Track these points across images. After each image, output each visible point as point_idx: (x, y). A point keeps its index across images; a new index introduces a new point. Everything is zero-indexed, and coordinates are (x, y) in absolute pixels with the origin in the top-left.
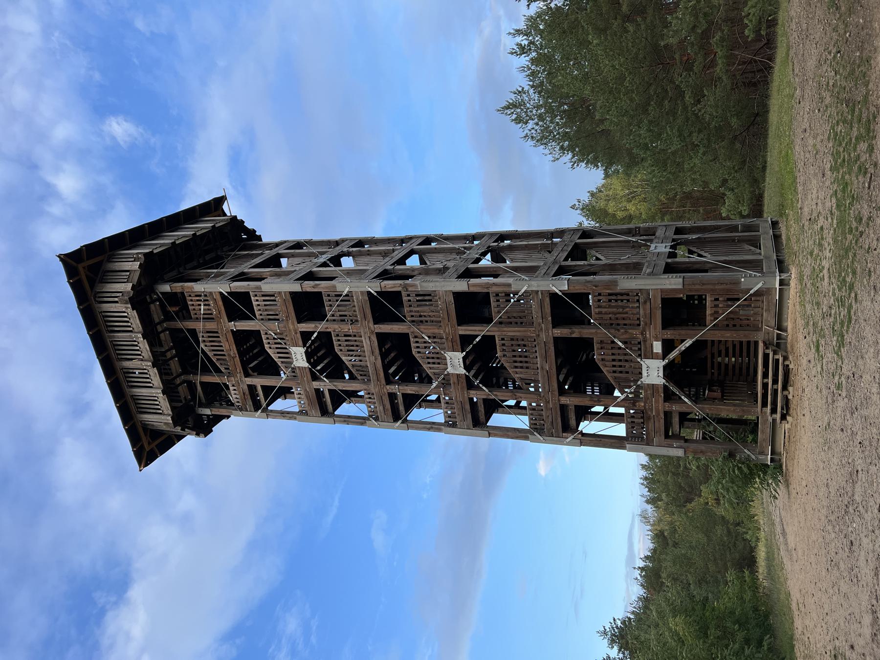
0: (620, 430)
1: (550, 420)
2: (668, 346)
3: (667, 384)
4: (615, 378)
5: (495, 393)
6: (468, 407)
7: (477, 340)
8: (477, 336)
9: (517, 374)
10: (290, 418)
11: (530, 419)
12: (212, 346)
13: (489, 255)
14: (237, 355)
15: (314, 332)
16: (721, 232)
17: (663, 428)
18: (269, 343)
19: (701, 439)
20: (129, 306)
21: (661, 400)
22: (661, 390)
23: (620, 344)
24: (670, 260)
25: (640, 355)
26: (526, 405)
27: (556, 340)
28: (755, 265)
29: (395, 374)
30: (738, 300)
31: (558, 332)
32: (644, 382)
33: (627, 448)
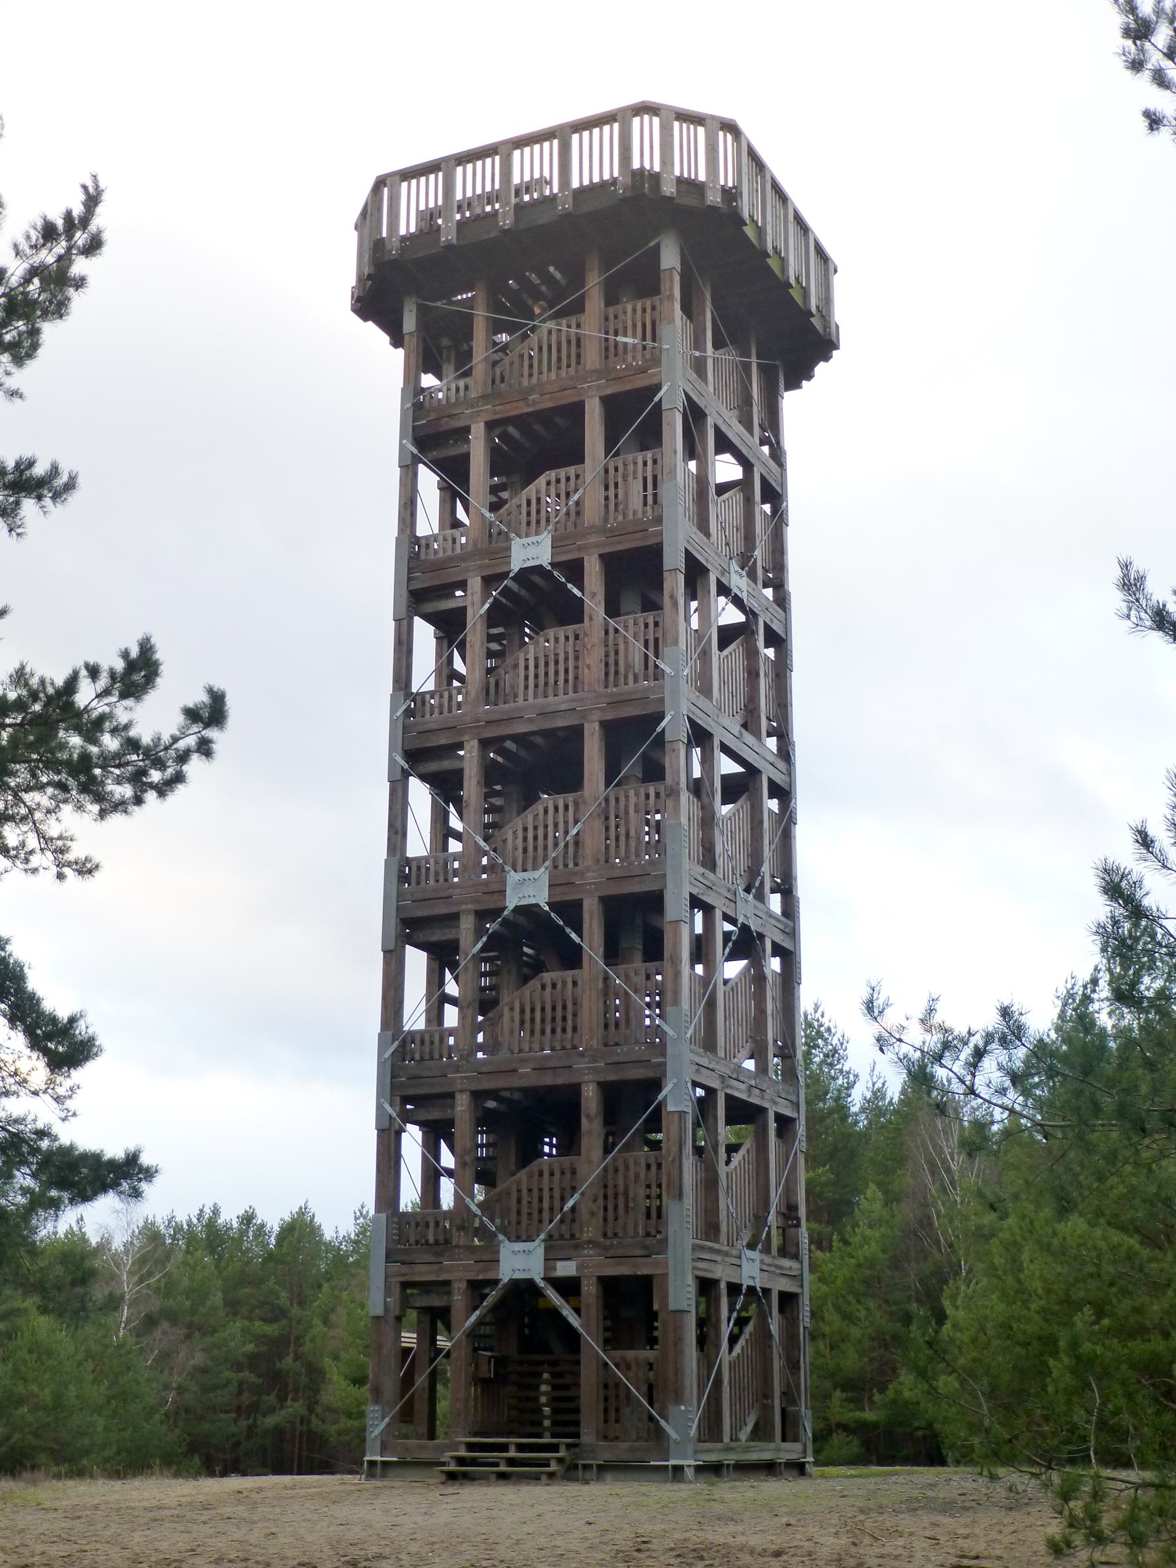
1: (424, 1074)
2: (569, 1288)
3: (500, 1286)
4: (508, 1194)
7: (573, 936)
8: (580, 935)
9: (512, 999)
10: (402, 520)
11: (421, 1033)
12: (550, 347)
14: (530, 409)
15: (582, 589)
17: (417, 1279)
18: (558, 481)
19: (403, 1345)
21: (472, 1276)
22: (490, 1276)
23: (570, 1203)
24: (723, 1286)
25: (550, 1237)
26: (450, 851)
27: (575, 1090)
28: (711, 1429)
29: (501, 751)
30: (651, 1405)
31: (590, 1096)
32: (502, 1245)
33: (380, 1215)
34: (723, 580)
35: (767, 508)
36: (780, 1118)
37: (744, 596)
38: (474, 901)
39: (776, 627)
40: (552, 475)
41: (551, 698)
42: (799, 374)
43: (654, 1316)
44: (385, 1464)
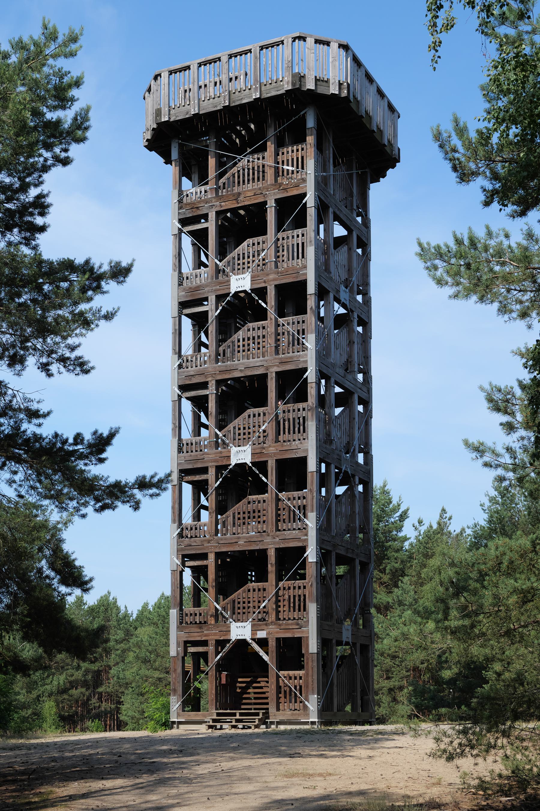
0: (187, 518)
2: (263, 643)
5: (214, 492)
6: (199, 465)
7: (264, 478)
13: (345, 312)
18: (254, 244)
21: (217, 638)
23: (263, 605)
27: (264, 552)
29: (227, 386)
31: (272, 554)
34: (337, 296)
35: (359, 251)
36: (361, 563)
37: (347, 303)
38: (215, 461)
40: (250, 241)
41: (251, 360)
43: (303, 656)
44: (180, 723)
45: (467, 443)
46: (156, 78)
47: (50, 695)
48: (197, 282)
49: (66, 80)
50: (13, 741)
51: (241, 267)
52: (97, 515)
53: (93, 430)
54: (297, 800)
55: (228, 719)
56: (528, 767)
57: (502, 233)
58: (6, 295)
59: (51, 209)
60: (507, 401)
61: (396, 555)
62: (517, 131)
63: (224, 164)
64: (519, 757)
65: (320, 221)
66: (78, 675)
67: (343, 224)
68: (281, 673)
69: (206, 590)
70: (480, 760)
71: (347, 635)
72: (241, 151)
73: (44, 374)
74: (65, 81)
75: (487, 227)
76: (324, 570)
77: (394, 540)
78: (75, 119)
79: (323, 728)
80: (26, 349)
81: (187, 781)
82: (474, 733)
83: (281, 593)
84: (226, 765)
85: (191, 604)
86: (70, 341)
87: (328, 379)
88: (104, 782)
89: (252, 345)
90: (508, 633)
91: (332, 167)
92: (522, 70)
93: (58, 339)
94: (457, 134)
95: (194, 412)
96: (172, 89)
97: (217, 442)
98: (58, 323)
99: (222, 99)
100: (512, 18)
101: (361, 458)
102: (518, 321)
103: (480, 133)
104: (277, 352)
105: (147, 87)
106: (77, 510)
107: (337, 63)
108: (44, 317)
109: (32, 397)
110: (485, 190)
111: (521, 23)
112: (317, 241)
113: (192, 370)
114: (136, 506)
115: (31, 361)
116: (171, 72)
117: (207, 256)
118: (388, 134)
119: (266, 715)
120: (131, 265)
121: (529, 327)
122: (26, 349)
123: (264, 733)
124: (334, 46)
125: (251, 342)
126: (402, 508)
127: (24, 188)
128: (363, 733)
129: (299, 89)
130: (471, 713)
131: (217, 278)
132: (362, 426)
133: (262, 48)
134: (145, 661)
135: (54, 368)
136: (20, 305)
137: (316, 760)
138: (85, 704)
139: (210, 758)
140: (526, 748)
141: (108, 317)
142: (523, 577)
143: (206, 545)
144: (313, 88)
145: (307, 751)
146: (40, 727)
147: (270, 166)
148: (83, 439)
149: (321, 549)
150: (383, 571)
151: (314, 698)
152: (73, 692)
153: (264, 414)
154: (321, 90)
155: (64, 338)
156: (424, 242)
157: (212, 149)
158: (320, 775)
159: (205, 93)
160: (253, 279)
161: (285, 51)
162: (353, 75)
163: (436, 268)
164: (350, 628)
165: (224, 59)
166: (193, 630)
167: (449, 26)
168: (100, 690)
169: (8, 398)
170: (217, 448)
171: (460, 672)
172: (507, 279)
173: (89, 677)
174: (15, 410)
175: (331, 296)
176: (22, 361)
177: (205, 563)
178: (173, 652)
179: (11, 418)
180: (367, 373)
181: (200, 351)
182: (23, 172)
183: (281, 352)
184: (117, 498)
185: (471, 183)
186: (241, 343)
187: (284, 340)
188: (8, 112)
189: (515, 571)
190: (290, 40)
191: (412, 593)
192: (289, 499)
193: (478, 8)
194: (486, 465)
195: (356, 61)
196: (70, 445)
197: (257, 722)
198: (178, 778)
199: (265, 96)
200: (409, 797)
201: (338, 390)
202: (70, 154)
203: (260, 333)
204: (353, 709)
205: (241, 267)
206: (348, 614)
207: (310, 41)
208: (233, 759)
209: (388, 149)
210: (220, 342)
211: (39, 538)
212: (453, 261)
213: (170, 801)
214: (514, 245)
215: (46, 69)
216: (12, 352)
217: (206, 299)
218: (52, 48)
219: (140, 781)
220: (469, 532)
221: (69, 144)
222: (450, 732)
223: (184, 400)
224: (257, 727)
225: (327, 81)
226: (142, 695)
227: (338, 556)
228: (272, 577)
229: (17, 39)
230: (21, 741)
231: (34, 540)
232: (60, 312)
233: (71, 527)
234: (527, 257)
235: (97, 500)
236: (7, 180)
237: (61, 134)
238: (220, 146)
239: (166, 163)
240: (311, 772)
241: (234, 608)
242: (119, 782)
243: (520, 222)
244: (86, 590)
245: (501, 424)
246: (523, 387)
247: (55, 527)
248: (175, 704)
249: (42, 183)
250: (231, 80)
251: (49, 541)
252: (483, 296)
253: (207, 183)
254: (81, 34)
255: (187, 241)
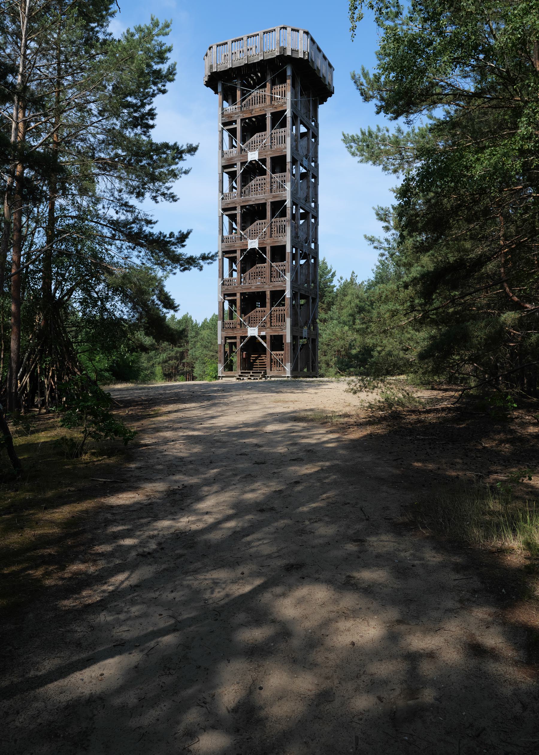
0: (226, 276)
2: (263, 338)
6: (232, 249)
16: (312, 357)
20: (278, 54)
21: (241, 335)
27: (264, 293)
29: (246, 209)
31: (268, 294)
35: (313, 140)
36: (312, 298)
37: (307, 167)
39: (315, 174)
40: (258, 134)
42: (323, 100)
43: (283, 344)
44: (223, 377)
45: (365, 237)
46: (210, 49)
47: (159, 364)
48: (231, 156)
49: (164, 48)
50: (141, 386)
51: (253, 148)
52: (181, 273)
53: (179, 230)
54: (280, 413)
55: (247, 375)
56: (393, 397)
57: (385, 129)
58: (134, 161)
59: (157, 117)
60: (386, 215)
61: (329, 294)
62: (394, 75)
63: (245, 94)
64: (388, 392)
65: (293, 124)
66: (173, 354)
67: (305, 126)
68: (272, 353)
69: (236, 311)
70: (369, 394)
71: (305, 334)
72: (253, 87)
73: (154, 202)
74: (163, 48)
75: (378, 126)
76: (294, 302)
77: (329, 287)
78: (169, 69)
79: (293, 379)
80: (144, 189)
81: (226, 404)
82: (367, 381)
83: (272, 313)
84: (245, 397)
85: (228, 318)
86: (167, 185)
87: (296, 205)
88: (186, 405)
89: (259, 188)
90: (385, 332)
91: (299, 96)
92: (397, 43)
93: (161, 184)
94: (363, 77)
95: (230, 222)
96: (218, 54)
97: (241, 237)
98: (161, 175)
99: (244, 60)
100: (392, 16)
101: (313, 246)
102: (392, 174)
103: (375, 75)
104: (271, 192)
105: (205, 54)
106: (171, 271)
107: (303, 42)
108: (154, 172)
109: (148, 213)
110: (377, 106)
111: (397, 19)
112: (292, 135)
113: (228, 201)
114: (201, 269)
115: (148, 195)
116: (218, 46)
117: (236, 142)
118: (328, 79)
119: (265, 373)
120: (198, 146)
121: (398, 178)
122: (144, 189)
123: (264, 382)
124: (301, 32)
125: (258, 186)
126: (333, 271)
127: (143, 105)
128: (312, 381)
129: (283, 55)
130: (366, 371)
131: (241, 153)
132: (314, 230)
133: (264, 33)
134: (205, 347)
135: (159, 198)
136: (141, 166)
137: (289, 394)
138: (176, 368)
139: (237, 393)
140: (392, 389)
141: (186, 172)
142: (392, 303)
143: (236, 289)
144: (290, 54)
145: (285, 390)
146: (154, 379)
147: (268, 96)
148: (174, 235)
149: (293, 291)
150: (323, 303)
151: (288, 365)
152: (170, 362)
153: (265, 223)
154: (294, 56)
155: (164, 183)
156: (346, 133)
157: (239, 86)
158: (292, 401)
159: (235, 56)
160: (259, 154)
161: (276, 35)
162: (311, 48)
163: (351, 147)
164: (307, 330)
165: (245, 39)
166: (229, 331)
167: (360, 18)
168: (184, 361)
169: (136, 214)
170: (241, 240)
171: (361, 351)
172: (387, 153)
173: (178, 355)
174: (140, 220)
175: (299, 163)
176: (143, 195)
177: (235, 298)
178: (219, 342)
179: (137, 224)
180: (316, 202)
181: (232, 191)
182: (142, 97)
183: (273, 191)
184: (191, 265)
185: (370, 102)
186: (253, 187)
187: (275, 186)
188: (134, 65)
189: (388, 300)
190: (279, 29)
191: (338, 313)
192: (277, 266)
193: (375, 9)
194: (375, 248)
195: (312, 40)
196: (168, 238)
197: (261, 376)
198: (222, 403)
199: (266, 58)
200: (334, 412)
201: (302, 211)
202: (166, 88)
203: (263, 182)
204: (307, 370)
205: (253, 148)
206: (306, 323)
207: (289, 29)
208: (249, 394)
209: (328, 87)
210: (243, 186)
211: (152, 284)
212: (360, 143)
213: (218, 414)
214: (391, 135)
215: (153, 42)
216: (138, 190)
217: (236, 164)
218: (156, 31)
219: (204, 404)
220: (366, 283)
221: (166, 82)
222: (355, 380)
223: (225, 216)
224: (260, 379)
225: (298, 51)
226: (204, 363)
227: (301, 295)
228: (268, 305)
229: (138, 26)
230: (145, 386)
231: (150, 285)
232: (162, 170)
233: (168, 279)
234: (397, 142)
235: (181, 265)
236: (134, 101)
237: (162, 77)
238: (243, 85)
239: (215, 93)
240: (287, 400)
241: (249, 320)
242: (193, 405)
243: (395, 122)
244: (176, 311)
245: (383, 227)
246: (394, 208)
247: (160, 279)
248: (220, 368)
249: (152, 103)
250: (248, 50)
251: (157, 286)
252: (375, 162)
253: (236, 104)
254: (171, 23)
255: (226, 134)
